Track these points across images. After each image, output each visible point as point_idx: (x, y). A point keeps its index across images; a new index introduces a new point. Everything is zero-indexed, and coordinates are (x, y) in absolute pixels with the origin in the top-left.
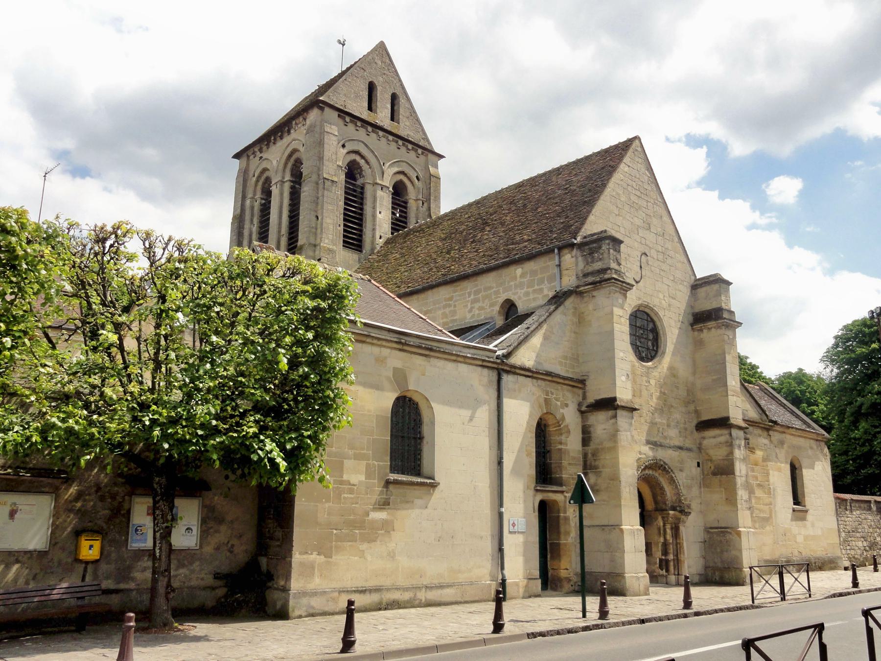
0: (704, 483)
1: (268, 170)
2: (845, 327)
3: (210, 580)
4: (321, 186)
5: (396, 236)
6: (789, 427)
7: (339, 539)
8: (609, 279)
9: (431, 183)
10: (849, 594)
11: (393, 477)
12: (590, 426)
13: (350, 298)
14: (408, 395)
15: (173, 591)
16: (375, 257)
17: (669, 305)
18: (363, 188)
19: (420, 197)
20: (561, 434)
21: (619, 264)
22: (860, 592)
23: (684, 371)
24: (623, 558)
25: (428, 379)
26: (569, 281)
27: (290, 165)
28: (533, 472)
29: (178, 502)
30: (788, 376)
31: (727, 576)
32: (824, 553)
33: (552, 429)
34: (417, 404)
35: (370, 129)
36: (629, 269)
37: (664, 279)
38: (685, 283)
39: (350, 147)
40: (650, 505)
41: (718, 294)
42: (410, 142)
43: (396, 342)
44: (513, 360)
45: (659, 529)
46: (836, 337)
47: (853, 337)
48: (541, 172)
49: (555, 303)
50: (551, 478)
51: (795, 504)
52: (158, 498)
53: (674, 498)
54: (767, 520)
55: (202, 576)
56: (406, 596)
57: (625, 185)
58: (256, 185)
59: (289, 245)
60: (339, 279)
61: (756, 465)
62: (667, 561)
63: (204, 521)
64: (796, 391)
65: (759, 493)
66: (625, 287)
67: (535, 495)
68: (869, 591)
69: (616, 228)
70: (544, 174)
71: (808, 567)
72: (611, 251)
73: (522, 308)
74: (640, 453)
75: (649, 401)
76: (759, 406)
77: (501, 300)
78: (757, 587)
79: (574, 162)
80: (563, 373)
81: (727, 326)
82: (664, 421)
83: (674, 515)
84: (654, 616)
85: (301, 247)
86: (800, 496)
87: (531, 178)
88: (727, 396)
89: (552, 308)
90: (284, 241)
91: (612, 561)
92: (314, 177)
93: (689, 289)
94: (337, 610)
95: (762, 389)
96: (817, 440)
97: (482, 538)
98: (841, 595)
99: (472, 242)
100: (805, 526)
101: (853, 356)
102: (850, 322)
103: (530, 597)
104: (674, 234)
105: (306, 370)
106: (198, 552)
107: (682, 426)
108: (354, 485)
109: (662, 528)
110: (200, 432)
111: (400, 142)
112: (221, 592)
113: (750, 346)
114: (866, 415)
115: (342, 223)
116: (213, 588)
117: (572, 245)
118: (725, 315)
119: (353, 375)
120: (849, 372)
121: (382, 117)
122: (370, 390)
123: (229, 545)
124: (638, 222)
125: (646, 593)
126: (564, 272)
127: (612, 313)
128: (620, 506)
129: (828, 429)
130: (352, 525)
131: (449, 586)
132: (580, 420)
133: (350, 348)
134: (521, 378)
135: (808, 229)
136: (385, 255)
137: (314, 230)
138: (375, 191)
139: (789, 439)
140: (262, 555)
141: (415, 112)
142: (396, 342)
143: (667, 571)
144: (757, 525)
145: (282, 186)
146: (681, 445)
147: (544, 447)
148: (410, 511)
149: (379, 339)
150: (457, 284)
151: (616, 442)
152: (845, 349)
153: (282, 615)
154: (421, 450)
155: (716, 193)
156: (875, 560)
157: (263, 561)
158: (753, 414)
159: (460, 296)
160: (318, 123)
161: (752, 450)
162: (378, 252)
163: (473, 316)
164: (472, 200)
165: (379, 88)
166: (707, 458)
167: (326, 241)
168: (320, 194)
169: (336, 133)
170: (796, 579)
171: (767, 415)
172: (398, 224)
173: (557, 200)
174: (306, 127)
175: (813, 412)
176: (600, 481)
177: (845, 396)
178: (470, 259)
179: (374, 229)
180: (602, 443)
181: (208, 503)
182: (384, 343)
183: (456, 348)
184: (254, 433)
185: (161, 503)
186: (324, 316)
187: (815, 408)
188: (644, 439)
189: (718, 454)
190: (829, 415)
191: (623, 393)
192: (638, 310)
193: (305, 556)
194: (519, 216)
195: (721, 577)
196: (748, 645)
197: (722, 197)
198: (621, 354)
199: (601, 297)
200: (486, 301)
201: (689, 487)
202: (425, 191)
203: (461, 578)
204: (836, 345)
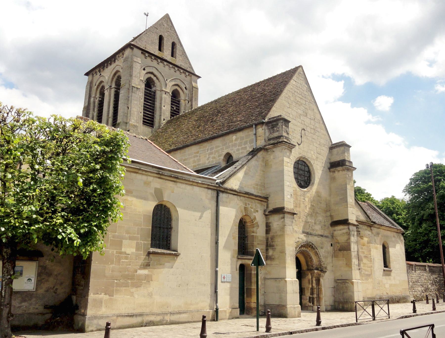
0: (335, 255)
1: (103, 82)
2: (415, 174)
3: (41, 309)
4: (131, 91)
5: (173, 119)
6: (382, 225)
7: (118, 285)
8: (282, 142)
9: (193, 91)
10: (411, 316)
11: (152, 250)
12: (270, 223)
13: (124, 146)
14: (164, 203)
15: (12, 316)
16: (160, 130)
17: (317, 158)
18: (155, 93)
19: (187, 98)
20: (254, 227)
21: (288, 134)
22: (417, 315)
23: (324, 194)
24: (286, 296)
25: (175, 195)
26: (261, 143)
27: (115, 80)
28: (236, 248)
29: (18, 263)
30: (387, 199)
31: (345, 306)
32: (400, 294)
33: (248, 224)
34: (169, 209)
35: (159, 60)
36: (294, 138)
37: (314, 143)
39: (148, 70)
40: (304, 267)
43: (156, 173)
44: (227, 185)
45: (309, 280)
46: (411, 179)
47: (419, 179)
48: (250, 85)
49: (252, 154)
50: (247, 252)
51: (385, 267)
52: (5, 261)
53: (318, 263)
55: (37, 306)
56: (158, 318)
57: (293, 92)
59: (113, 123)
60: (117, 135)
61: (364, 245)
62: (313, 298)
63: (39, 275)
64: (389, 209)
65: (365, 261)
66: (291, 146)
67: (237, 261)
68: (422, 315)
69: (288, 115)
70: (251, 86)
71: (389, 302)
72: (284, 126)
73: (235, 157)
74: (299, 238)
75: (304, 209)
76: (366, 213)
78: (359, 313)
79: (267, 80)
80: (255, 193)
81: (348, 170)
82: (313, 221)
83: (317, 272)
84: (298, 330)
85: (119, 124)
86: (388, 262)
87: (244, 88)
88: (347, 207)
89: (250, 157)
90: (111, 120)
91: (280, 298)
92: (127, 86)
93: (328, 149)
94: (115, 327)
95: (369, 205)
96: (397, 232)
97: (205, 285)
98: (406, 317)
99: (211, 122)
100: (390, 279)
101: (419, 189)
102: (418, 171)
103: (233, 318)
104: (320, 119)
105: (95, 186)
106: (35, 293)
107: (323, 224)
108: (128, 254)
110: (25, 222)
111: (176, 69)
112: (48, 316)
113: (360, 180)
114: (426, 220)
115: (142, 111)
116: (43, 314)
117: (263, 123)
118: (347, 164)
119: (124, 191)
120: (418, 197)
121: (166, 54)
122: (140, 200)
123: (55, 289)
124: (300, 112)
125: (299, 316)
126: (258, 138)
127: (283, 161)
128: (285, 267)
129: (406, 228)
130: (126, 277)
132: (265, 219)
133: (123, 175)
134: (231, 196)
135: (397, 124)
136: (166, 129)
137: (126, 115)
138: (161, 94)
139: (382, 232)
140: (74, 295)
141: (185, 53)
142: (156, 173)
143: (313, 303)
145: (110, 90)
146: (322, 234)
147: (244, 234)
148: (162, 269)
149: (146, 171)
150: (202, 144)
151: (284, 232)
152: (415, 185)
153: (82, 330)
154: (170, 235)
155: (350, 104)
156: (427, 297)
157: (74, 298)
158: (362, 218)
160: (130, 56)
161: (362, 237)
162: (163, 128)
163: (209, 162)
164: (213, 100)
165: (165, 39)
166: (336, 241)
167: (133, 121)
168: (130, 95)
169: (140, 62)
170: (382, 308)
171: (370, 219)
172: (175, 112)
173: (257, 99)
174: (124, 58)
175: (399, 219)
176: (275, 253)
177: (415, 210)
178: (209, 131)
179: (160, 115)
180: (276, 232)
181: (42, 264)
182: (149, 174)
183: (192, 177)
184: (60, 223)
185: (7, 264)
186: (107, 156)
187: (400, 217)
188: (301, 231)
189: (342, 239)
190: (407, 220)
191: (289, 205)
192: (299, 160)
193: (97, 296)
194: (236, 108)
195: (343, 307)
196: (403, 333)
197: (352, 106)
198: (288, 183)
199: (278, 152)
200: (217, 153)
201: (326, 257)
202: (190, 95)
203: (192, 308)
204: (411, 183)
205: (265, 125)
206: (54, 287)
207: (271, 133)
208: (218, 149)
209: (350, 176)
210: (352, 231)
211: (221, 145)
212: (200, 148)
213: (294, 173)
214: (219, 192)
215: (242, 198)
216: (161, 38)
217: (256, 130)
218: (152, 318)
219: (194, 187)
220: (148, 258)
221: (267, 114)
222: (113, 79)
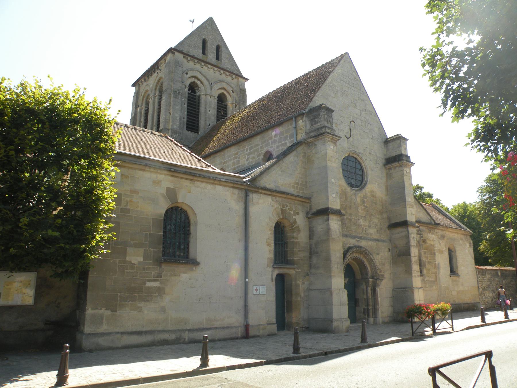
8: (324, 133)
14: (179, 205)
20: (294, 232)
24: (331, 309)
26: (301, 136)
33: (288, 229)
34: (186, 212)
35: (203, 64)
39: (190, 74)
41: (400, 146)
58: (143, 100)
61: (427, 250)
65: (428, 267)
67: (273, 271)
77: (263, 152)
80: (295, 193)
88: (406, 207)
90: (142, 124)
94: (120, 346)
108: (134, 264)
111: (222, 71)
115: (186, 117)
117: (303, 114)
126: (299, 131)
139: (448, 234)
143: (368, 316)
158: (424, 218)
159: (241, 151)
189: (401, 243)
193: (96, 311)
206: (56, 301)
207: (312, 125)
208: (257, 148)
212: (239, 149)
213: (343, 170)
215: (278, 199)
216: (204, 42)
217: (296, 123)
219: (217, 186)
222: (156, 86)
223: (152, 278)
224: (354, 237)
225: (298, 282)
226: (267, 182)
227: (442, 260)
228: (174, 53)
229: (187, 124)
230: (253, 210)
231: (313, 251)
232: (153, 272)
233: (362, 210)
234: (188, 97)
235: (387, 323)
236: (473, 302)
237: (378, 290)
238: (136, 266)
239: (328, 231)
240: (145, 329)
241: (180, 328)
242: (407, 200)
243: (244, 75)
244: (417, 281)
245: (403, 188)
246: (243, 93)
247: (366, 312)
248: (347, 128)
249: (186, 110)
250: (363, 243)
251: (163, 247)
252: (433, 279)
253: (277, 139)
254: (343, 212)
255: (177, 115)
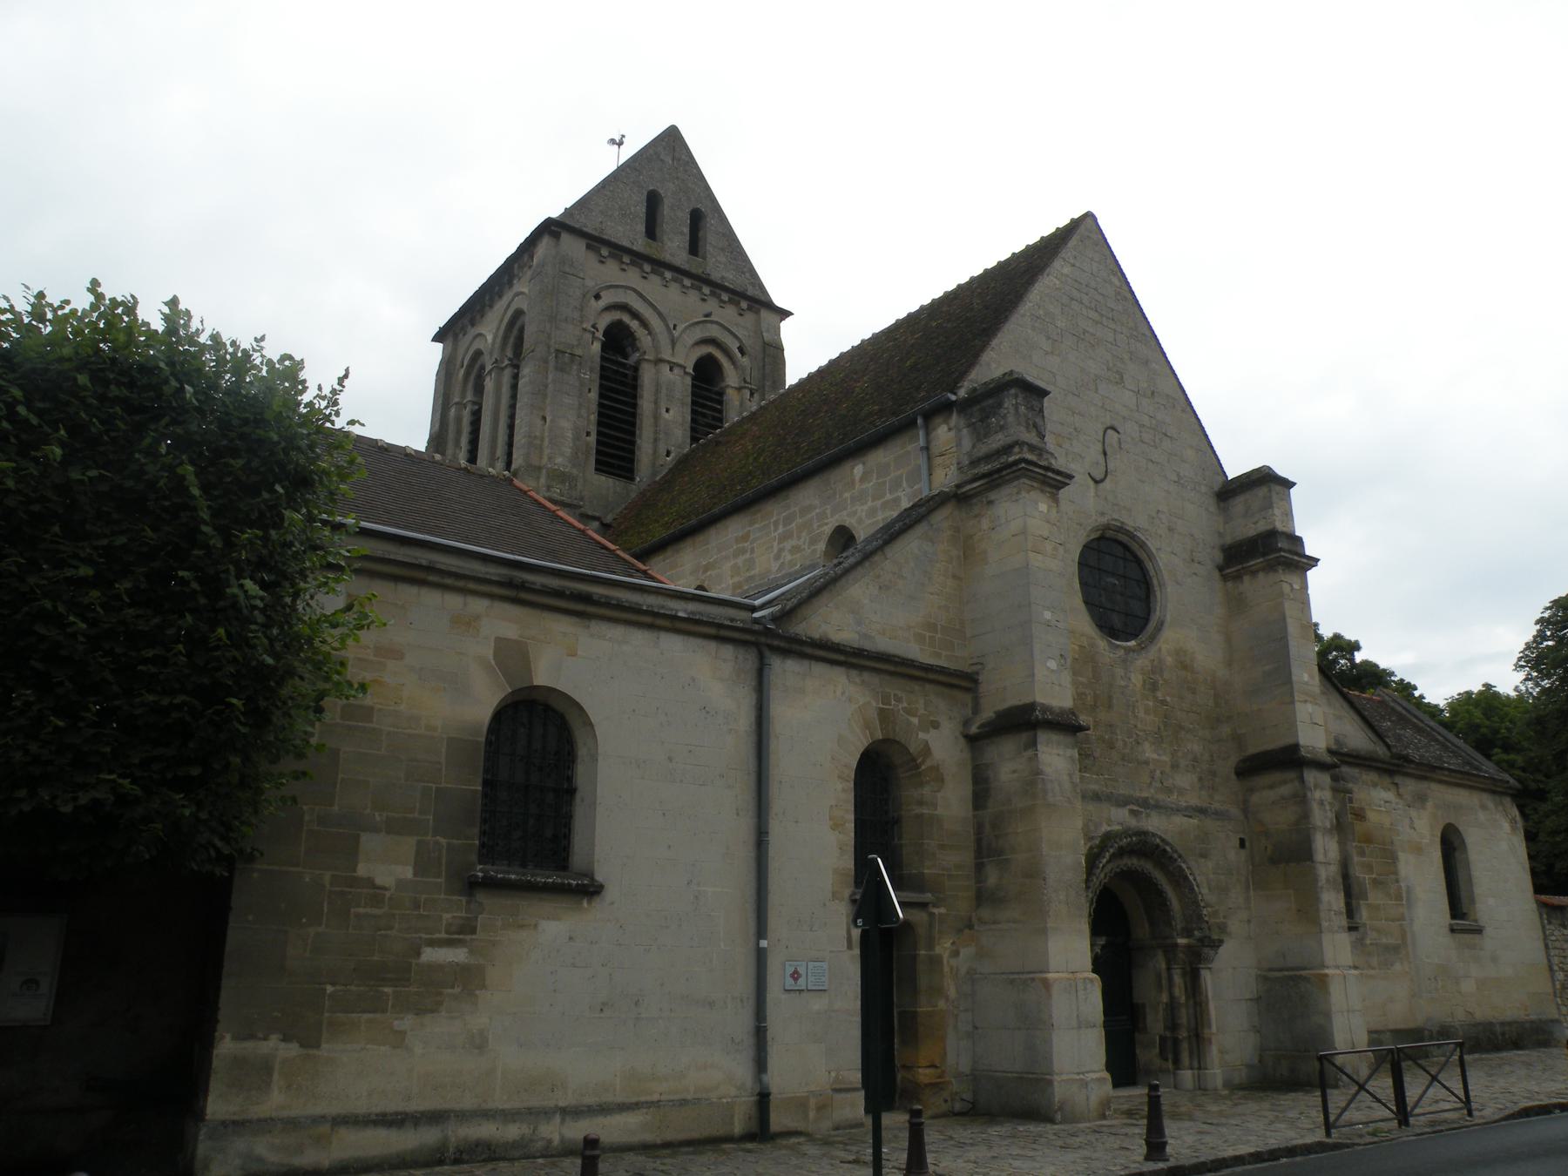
8: (1016, 463)
18: (636, 369)
26: (945, 477)
35: (647, 267)
36: (1071, 450)
38: (1203, 489)
39: (608, 298)
42: (726, 289)
45: (1159, 976)
54: (1395, 951)
65: (1375, 897)
77: (828, 530)
88: (1293, 702)
97: (711, 1004)
108: (386, 889)
109: (1164, 975)
115: (593, 429)
117: (946, 408)
126: (938, 461)
131: (623, 1108)
143: (1177, 1062)
144: (1374, 961)
158: (1357, 737)
182: (472, 586)
189: (1280, 819)
192: (1101, 538)
205: (959, 412)
209: (1296, 587)
210: (1316, 786)
211: (817, 502)
214: (767, 653)
215: (866, 676)
216: (653, 201)
217: (927, 434)
218: (487, 1131)
220: (468, 903)
221: (963, 374)
223: (443, 935)
224: (1122, 802)
225: (938, 950)
226: (832, 621)
227: (1422, 876)
228: (556, 236)
229: (598, 452)
230: (783, 713)
231: (987, 845)
232: (447, 916)
233: (1147, 712)
234: (602, 368)
235: (1242, 1087)
236: (1533, 1017)
237: (1207, 977)
238: (388, 894)
239: (1033, 781)
240: (414, 1106)
241: (535, 1102)
242: (1294, 678)
243: (779, 300)
244: (1337, 948)
245: (1283, 640)
246: (773, 354)
247: (1170, 1049)
248: (1094, 452)
249: (594, 407)
250: (1154, 824)
251: (483, 833)
252: (1391, 941)
253: (867, 493)
254: (1084, 719)
255: (567, 425)
